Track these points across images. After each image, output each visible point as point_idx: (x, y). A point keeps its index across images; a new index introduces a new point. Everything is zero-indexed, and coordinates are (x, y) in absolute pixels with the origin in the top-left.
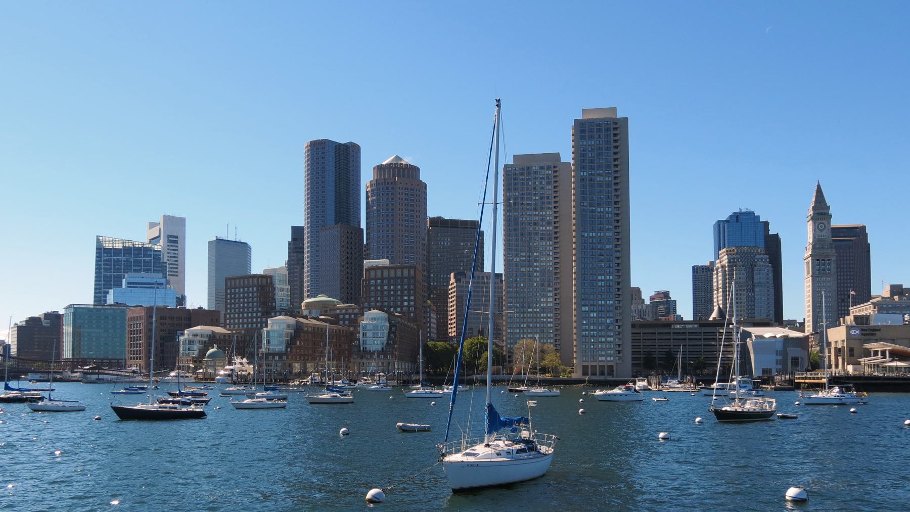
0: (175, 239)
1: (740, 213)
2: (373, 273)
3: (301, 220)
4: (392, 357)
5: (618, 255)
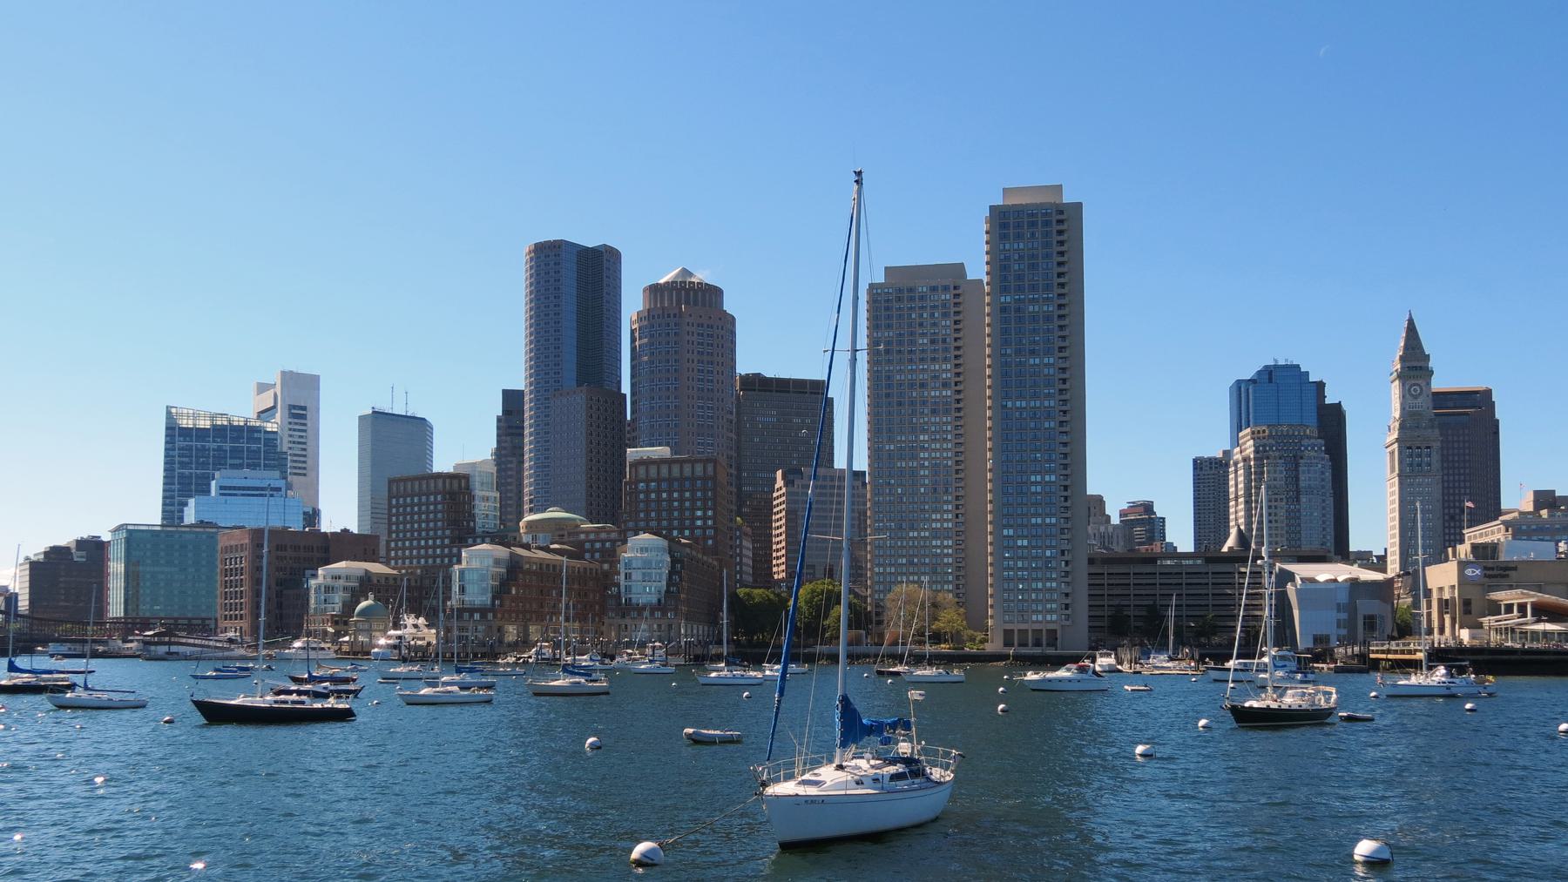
0: (302, 412)
1: (1276, 366)
2: (642, 470)
3: (518, 380)
4: (676, 615)
5: (1065, 438)
